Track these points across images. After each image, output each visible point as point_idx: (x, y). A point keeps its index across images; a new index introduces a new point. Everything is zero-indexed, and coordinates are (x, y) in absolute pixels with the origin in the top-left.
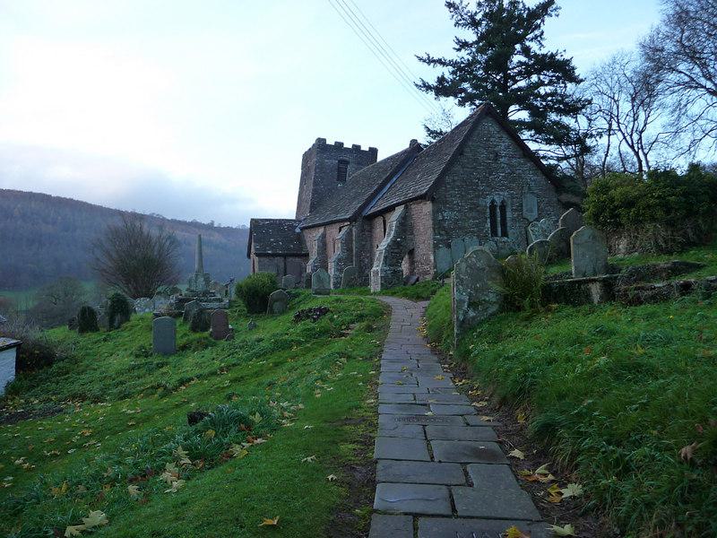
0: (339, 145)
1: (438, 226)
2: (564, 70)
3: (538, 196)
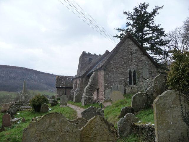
0: (90, 54)
1: (106, 80)
2: (160, 32)
3: (149, 69)
